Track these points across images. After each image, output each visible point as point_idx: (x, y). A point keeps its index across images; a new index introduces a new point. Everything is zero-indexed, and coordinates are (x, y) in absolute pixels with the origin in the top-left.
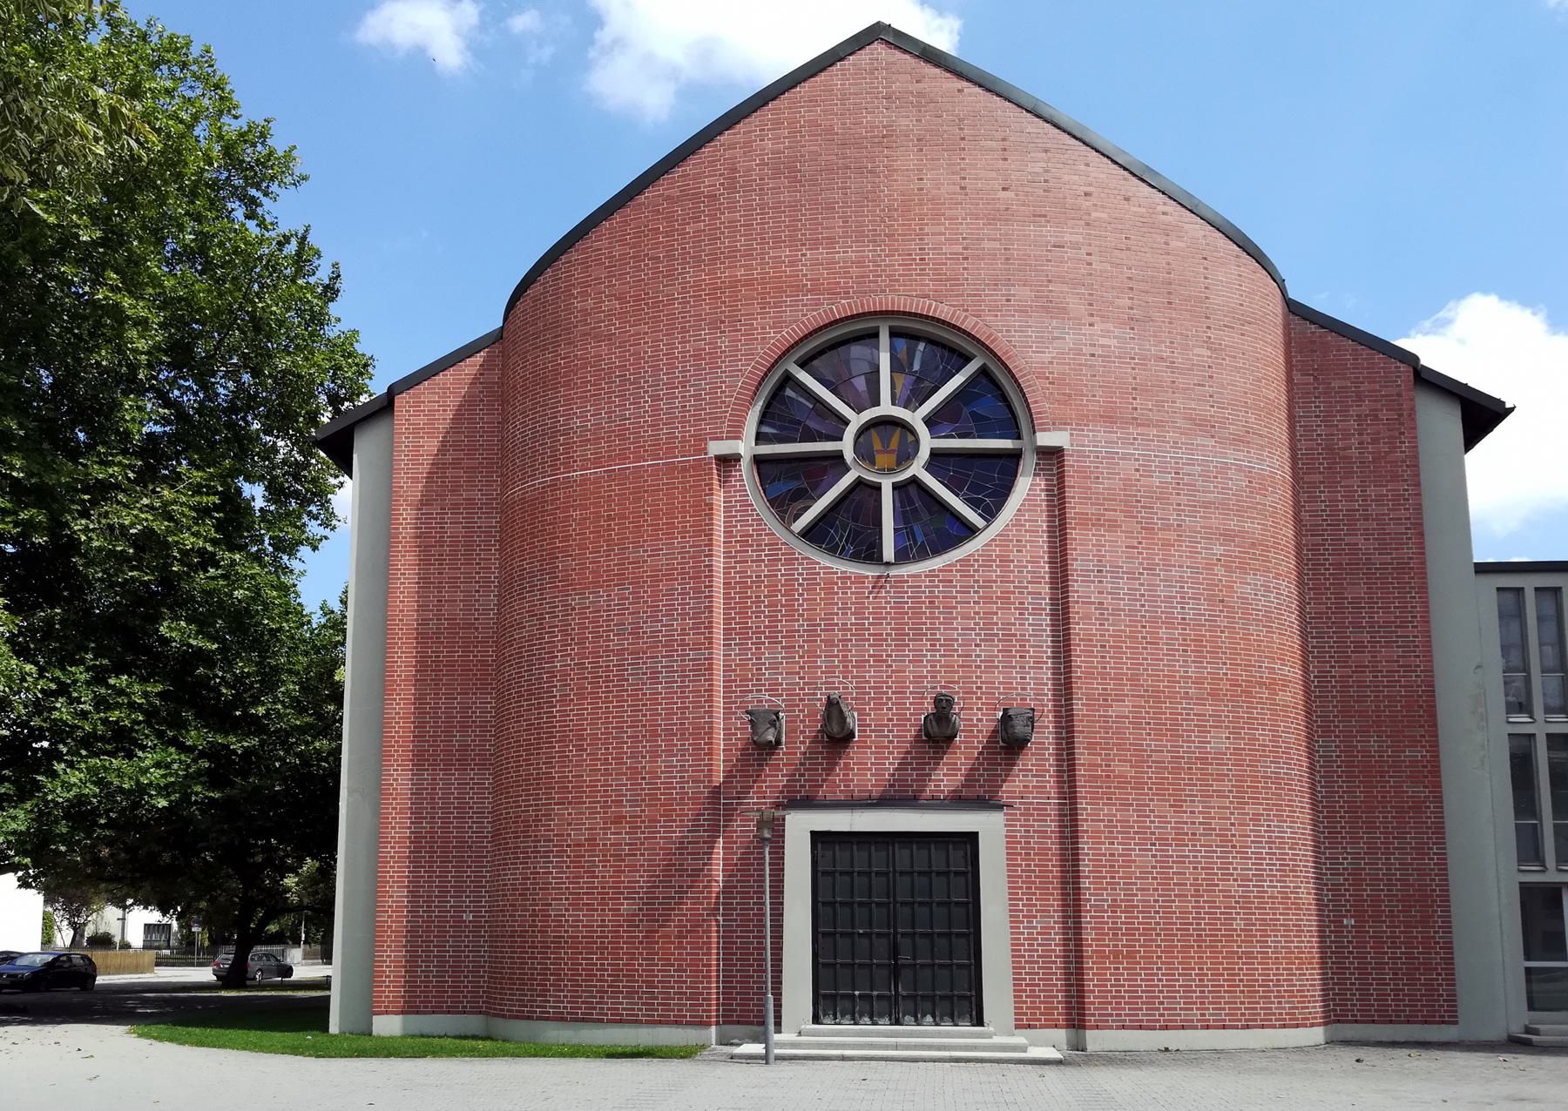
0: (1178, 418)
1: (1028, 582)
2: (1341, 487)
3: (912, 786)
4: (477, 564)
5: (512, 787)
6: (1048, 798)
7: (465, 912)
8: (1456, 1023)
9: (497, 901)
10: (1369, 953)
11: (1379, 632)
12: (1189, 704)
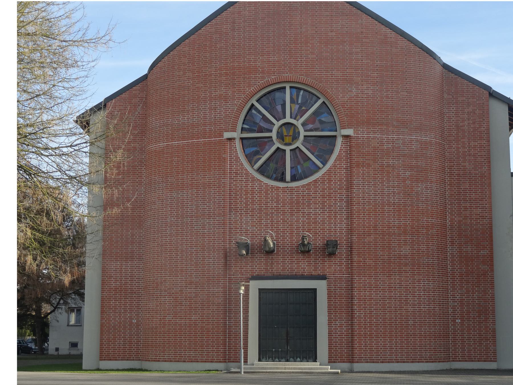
0: (394, 121)
1: (338, 189)
2: (461, 142)
3: (295, 270)
4: (137, 174)
5: (152, 269)
6: (343, 274)
7: (133, 319)
8: (496, 361)
9: (146, 315)
10: (465, 333)
11: (473, 203)
12: (395, 236)
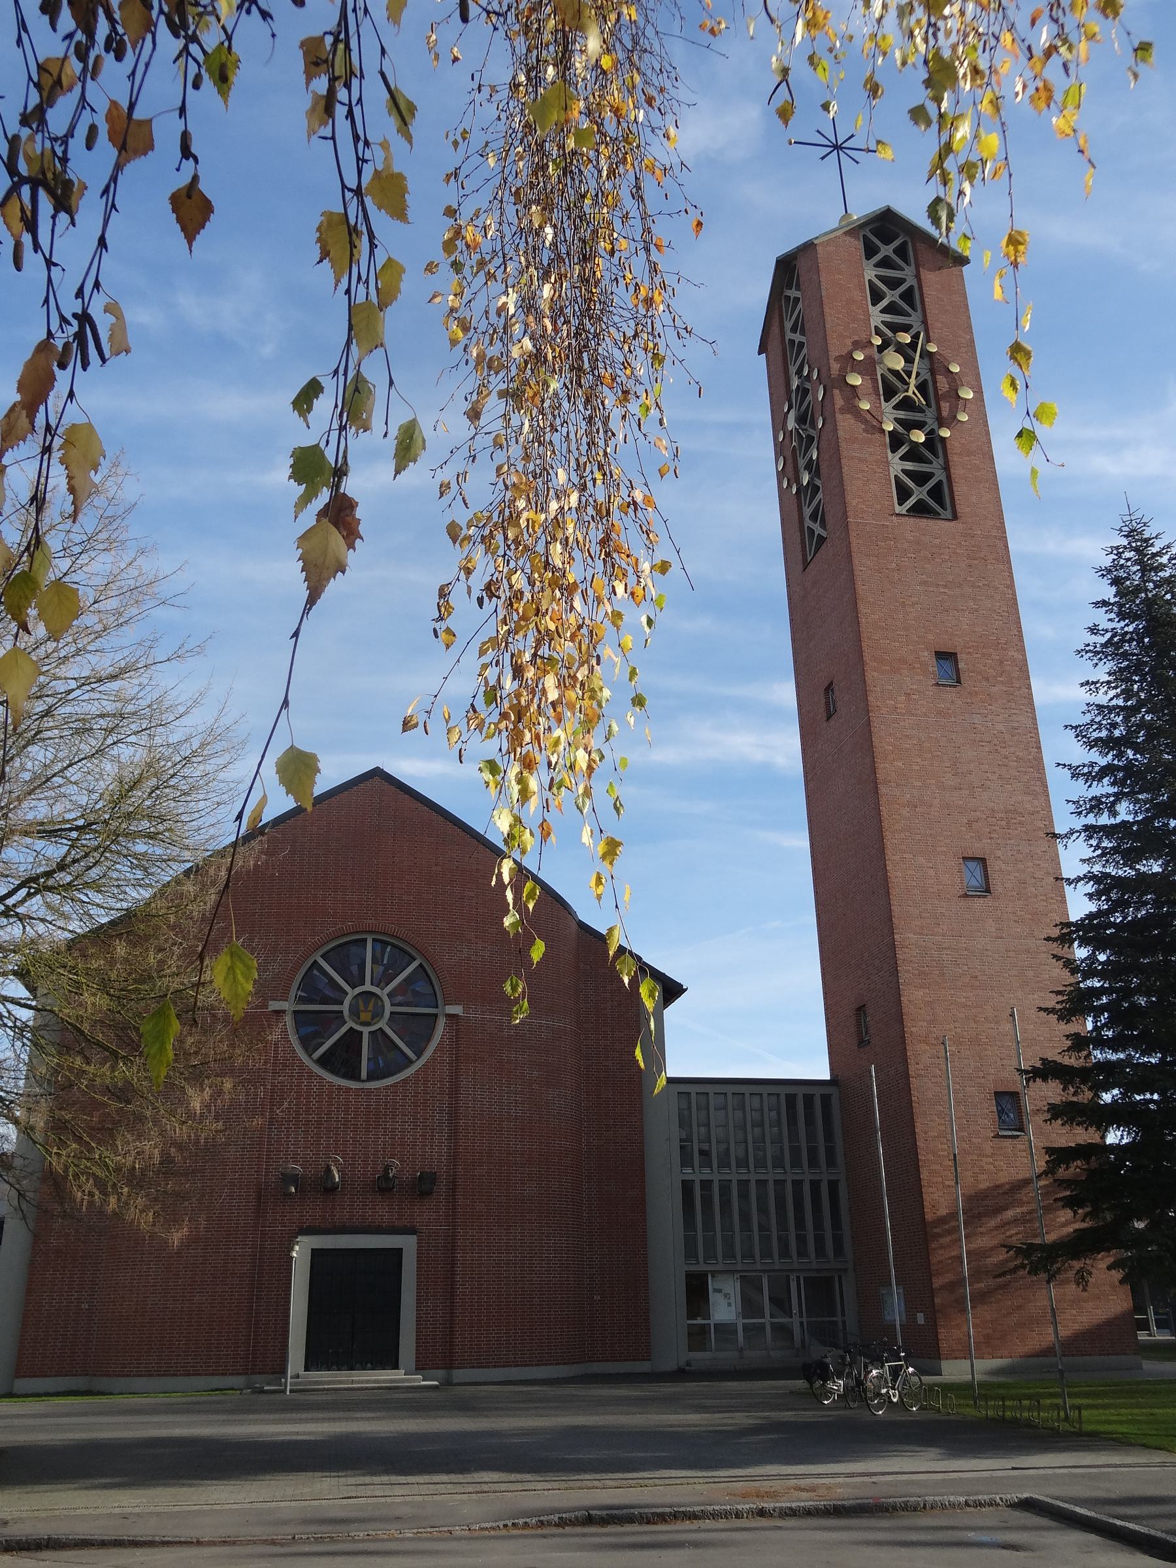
8: (650, 1360)
